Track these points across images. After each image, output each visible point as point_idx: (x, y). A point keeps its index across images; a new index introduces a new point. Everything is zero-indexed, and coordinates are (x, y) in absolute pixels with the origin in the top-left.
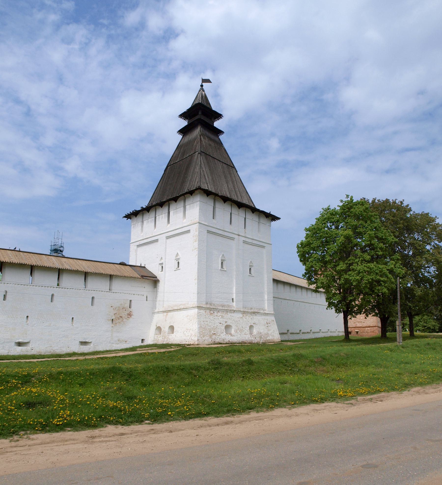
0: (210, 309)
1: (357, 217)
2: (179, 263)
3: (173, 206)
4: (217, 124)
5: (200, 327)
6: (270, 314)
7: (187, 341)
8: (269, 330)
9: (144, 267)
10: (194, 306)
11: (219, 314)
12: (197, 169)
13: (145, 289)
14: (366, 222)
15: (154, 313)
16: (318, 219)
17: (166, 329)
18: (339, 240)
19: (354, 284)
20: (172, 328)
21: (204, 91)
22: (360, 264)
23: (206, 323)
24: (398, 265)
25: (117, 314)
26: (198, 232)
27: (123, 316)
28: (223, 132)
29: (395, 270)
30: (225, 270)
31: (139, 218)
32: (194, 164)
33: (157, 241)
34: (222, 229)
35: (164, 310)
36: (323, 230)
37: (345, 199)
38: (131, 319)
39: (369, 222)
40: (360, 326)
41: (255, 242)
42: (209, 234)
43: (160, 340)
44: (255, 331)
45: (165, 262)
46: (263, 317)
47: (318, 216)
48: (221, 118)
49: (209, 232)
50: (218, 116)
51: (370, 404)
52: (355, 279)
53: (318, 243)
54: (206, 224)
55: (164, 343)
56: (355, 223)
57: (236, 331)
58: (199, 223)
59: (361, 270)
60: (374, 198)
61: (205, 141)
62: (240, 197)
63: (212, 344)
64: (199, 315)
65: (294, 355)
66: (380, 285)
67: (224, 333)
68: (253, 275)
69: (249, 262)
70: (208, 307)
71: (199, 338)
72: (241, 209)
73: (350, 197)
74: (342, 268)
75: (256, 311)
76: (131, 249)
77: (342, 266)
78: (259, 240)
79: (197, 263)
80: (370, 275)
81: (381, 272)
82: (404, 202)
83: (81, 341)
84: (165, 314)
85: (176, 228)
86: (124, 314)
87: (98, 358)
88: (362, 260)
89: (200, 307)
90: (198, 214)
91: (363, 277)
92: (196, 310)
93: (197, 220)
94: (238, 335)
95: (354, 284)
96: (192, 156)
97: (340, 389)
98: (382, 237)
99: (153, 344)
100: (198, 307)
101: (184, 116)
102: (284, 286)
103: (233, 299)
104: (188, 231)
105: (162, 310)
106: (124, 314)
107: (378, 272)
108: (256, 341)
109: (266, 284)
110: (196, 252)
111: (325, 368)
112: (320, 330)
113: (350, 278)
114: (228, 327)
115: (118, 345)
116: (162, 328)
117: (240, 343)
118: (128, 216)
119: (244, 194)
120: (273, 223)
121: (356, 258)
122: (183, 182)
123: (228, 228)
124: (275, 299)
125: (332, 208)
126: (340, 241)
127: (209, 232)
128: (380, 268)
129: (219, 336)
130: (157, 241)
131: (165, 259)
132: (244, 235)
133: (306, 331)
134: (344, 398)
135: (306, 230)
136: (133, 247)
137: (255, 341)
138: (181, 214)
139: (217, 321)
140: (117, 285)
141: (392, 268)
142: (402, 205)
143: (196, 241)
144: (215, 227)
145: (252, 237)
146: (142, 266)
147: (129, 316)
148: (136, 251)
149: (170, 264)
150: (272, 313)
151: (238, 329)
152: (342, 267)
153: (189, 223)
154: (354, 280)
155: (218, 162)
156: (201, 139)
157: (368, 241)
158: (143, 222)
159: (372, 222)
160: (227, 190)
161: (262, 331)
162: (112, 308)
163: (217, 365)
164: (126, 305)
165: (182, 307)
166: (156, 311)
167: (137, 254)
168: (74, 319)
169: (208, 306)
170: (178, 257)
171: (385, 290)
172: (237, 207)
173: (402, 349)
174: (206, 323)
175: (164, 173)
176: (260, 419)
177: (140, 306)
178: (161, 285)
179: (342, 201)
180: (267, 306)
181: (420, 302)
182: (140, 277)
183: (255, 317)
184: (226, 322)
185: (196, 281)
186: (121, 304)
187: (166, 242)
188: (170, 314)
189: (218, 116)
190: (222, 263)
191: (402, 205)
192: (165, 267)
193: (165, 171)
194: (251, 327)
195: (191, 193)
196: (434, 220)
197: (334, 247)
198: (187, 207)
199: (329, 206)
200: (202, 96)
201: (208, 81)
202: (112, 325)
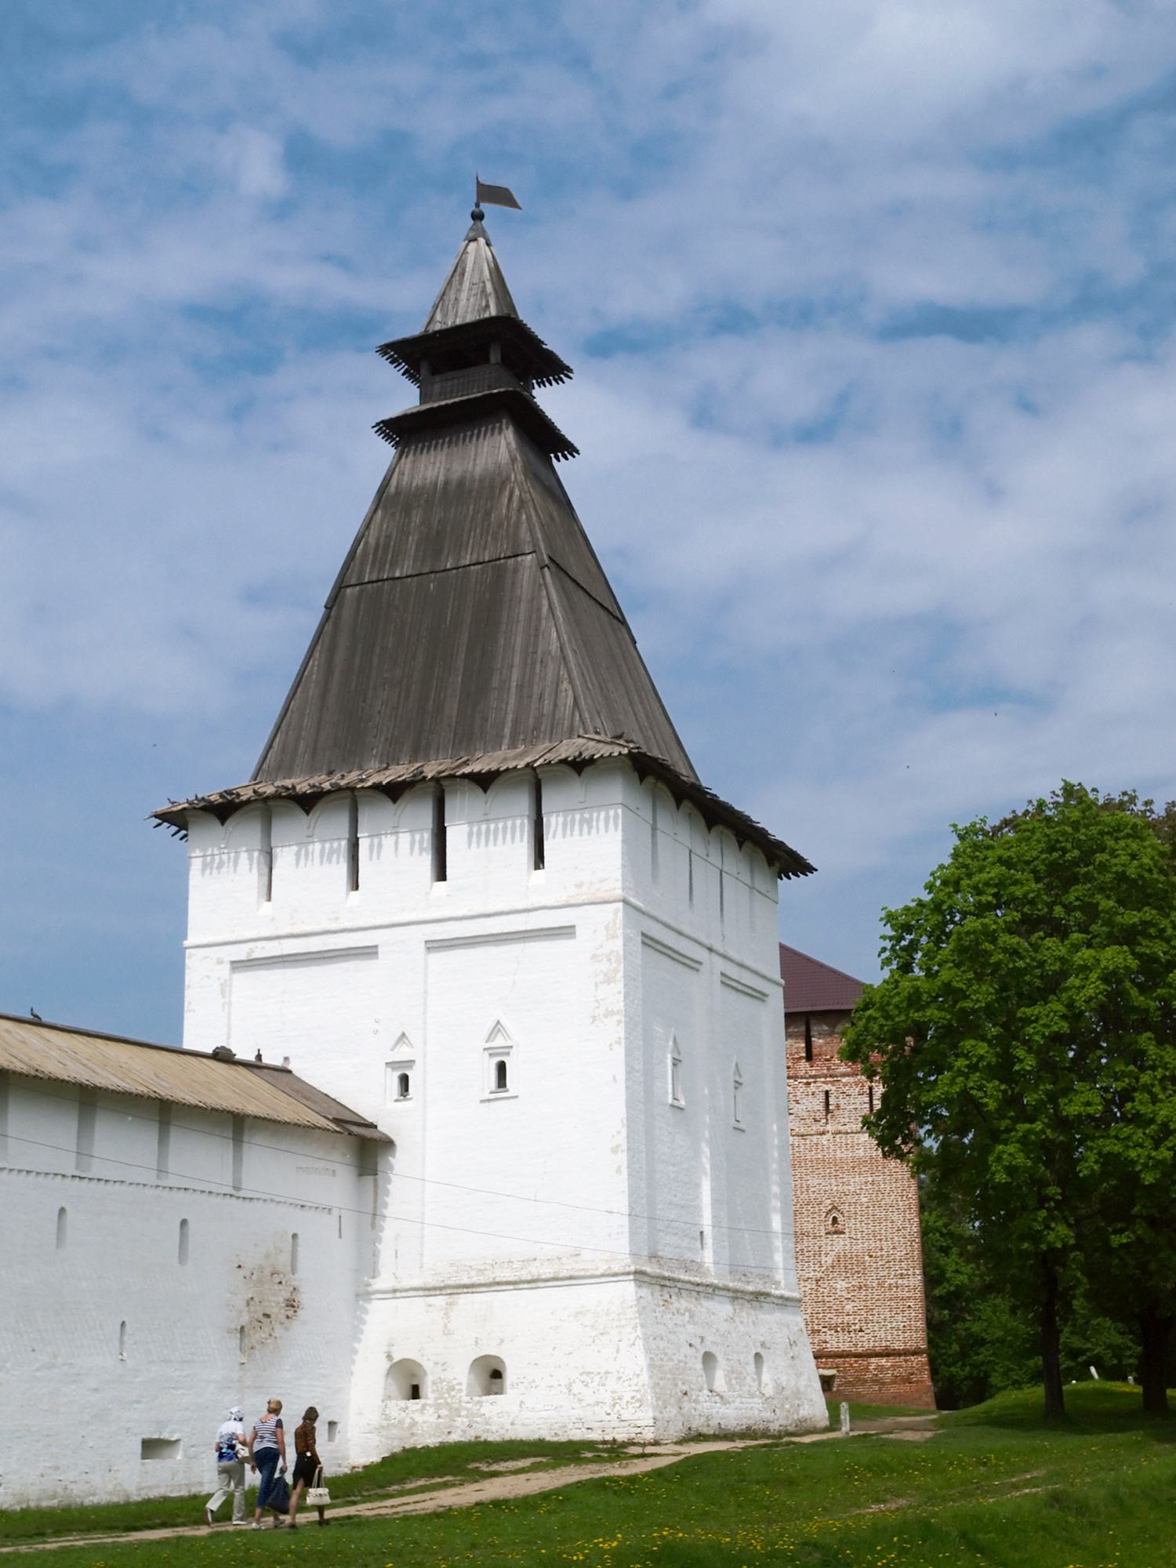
2: (502, 1068)
5: (652, 1366)
10: (616, 1268)
13: (329, 1179)
19: (1148, 1178)
20: (493, 1375)
40: (845, 1347)
42: (648, 949)
43: (428, 1425)
48: (559, 380)
52: (1150, 1157)
53: (983, 994)
54: (640, 904)
55: (455, 1437)
56: (1131, 918)
58: (625, 902)
70: (662, 1280)
71: (657, 1414)
83: (147, 1436)
84: (440, 1301)
85: (490, 909)
88: (1164, 1077)
92: (628, 1289)
95: (1148, 1178)
96: (498, 571)
100: (636, 1273)
104: (566, 932)
113: (1133, 1154)
118: (178, 819)
136: (202, 975)
143: (609, 980)
146: (266, 1060)
147: (291, 1313)
148: (225, 989)
149: (452, 1074)
152: (1088, 1104)
153: (563, 899)
154: (1145, 1165)
162: (242, 1272)
165: (547, 1271)
166: (378, 1284)
168: (128, 1329)
170: (499, 1041)
172: (703, 821)
175: (326, 618)
177: (322, 1269)
178: (400, 1164)
185: (622, 1158)
186: (267, 1256)
188: (464, 1300)
189: (553, 369)
193: (329, 607)
197: (1047, 1017)
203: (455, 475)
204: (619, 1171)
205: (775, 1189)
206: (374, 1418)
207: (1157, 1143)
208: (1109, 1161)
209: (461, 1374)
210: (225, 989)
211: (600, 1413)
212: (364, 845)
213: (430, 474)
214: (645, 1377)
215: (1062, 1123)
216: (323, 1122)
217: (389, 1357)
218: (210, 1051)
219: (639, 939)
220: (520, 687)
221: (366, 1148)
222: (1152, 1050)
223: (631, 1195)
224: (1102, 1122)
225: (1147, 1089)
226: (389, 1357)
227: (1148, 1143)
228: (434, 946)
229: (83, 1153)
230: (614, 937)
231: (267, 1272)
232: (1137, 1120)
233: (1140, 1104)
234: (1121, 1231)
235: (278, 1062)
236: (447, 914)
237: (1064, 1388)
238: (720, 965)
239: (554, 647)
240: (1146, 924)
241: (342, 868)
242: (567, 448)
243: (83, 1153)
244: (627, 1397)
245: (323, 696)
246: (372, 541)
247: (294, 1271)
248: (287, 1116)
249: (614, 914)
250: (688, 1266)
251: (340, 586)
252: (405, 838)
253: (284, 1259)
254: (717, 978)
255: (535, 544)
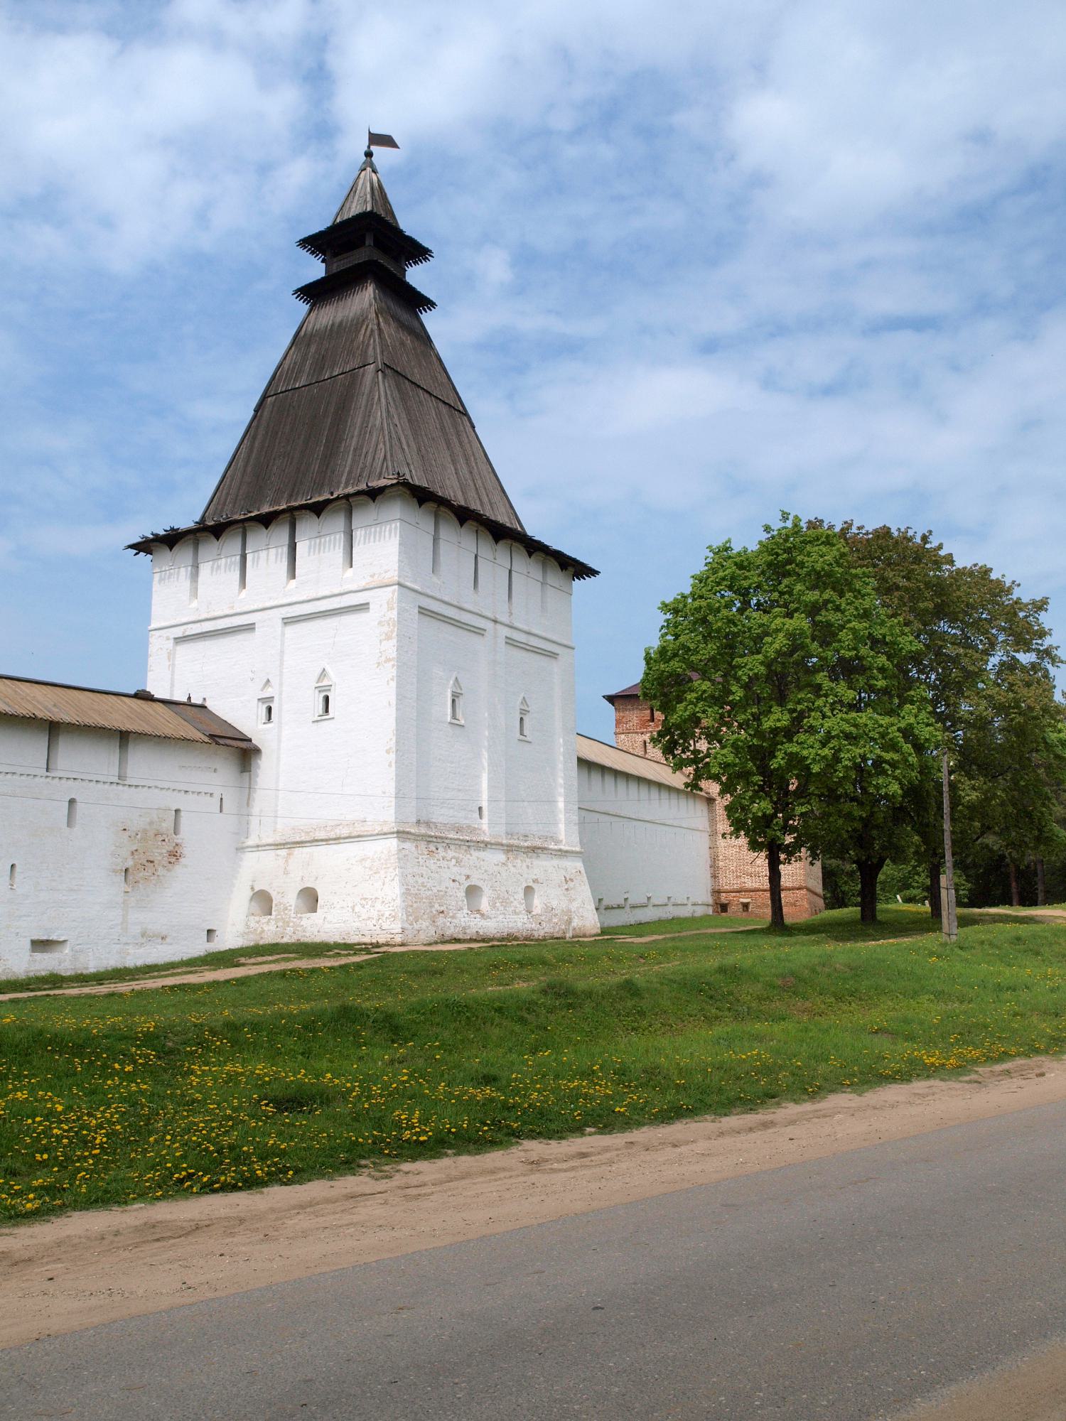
0: (428, 839)
1: (819, 580)
2: (327, 699)
3: (307, 530)
4: (416, 276)
5: (407, 893)
6: (572, 852)
7: (366, 933)
8: (571, 900)
9: (203, 707)
11: (451, 854)
12: (379, 416)
13: (215, 776)
14: (841, 595)
15: (241, 849)
16: (701, 579)
17: (287, 898)
18: (771, 644)
19: (816, 769)
20: (310, 899)
21: (374, 171)
22: (829, 714)
23: (420, 880)
24: (923, 715)
25: (141, 851)
26: (395, 612)
27: (157, 858)
28: (433, 304)
29: (916, 732)
30: (462, 722)
31: (183, 554)
32: (363, 401)
33: (250, 628)
34: (455, 603)
35: (278, 839)
36: (724, 612)
37: (777, 525)
38: (178, 869)
39: (849, 595)
41: (534, 642)
43: (270, 931)
44: (538, 904)
45: (281, 694)
46: (556, 862)
47: (699, 567)
48: (426, 259)
49: (423, 611)
50: (418, 252)
51: (1007, 1084)
53: (711, 649)
54: (416, 587)
56: (813, 596)
57: (494, 906)
58: (399, 584)
59: (833, 729)
60: (848, 520)
61: (390, 330)
62: (488, 507)
63: (436, 943)
64: (402, 857)
65: (722, 970)
66: (884, 772)
67: (466, 911)
68: (528, 739)
69: (520, 699)
70: (423, 835)
71: (406, 926)
72: (501, 543)
73: (791, 517)
74: (778, 724)
75: (538, 843)
76: (152, 649)
77: (778, 718)
78: (543, 634)
79: (394, 702)
80: (856, 745)
81: (883, 736)
82: (931, 538)
83: (35, 938)
84: (283, 852)
85: (320, 595)
86: (159, 853)
87: (172, 988)
88: (835, 702)
89: (404, 832)
90: (396, 558)
91: (840, 750)
92: (393, 843)
93: (393, 575)
94: (500, 917)
95: (816, 769)
96: (353, 376)
97: (897, 1052)
98: (884, 637)
99: (242, 949)
100: (398, 832)
101: (314, 243)
102: (589, 772)
103: (480, 808)
104: (363, 607)
105: (270, 841)
106: (159, 853)
107: (877, 736)
108: (542, 933)
109: (560, 766)
110: (391, 671)
111: (808, 1004)
112: (649, 898)
113: (805, 753)
114: (472, 892)
115: (142, 950)
116: (274, 894)
117: (503, 939)
118: (144, 546)
119: (497, 497)
120: (577, 583)
121: (819, 696)
122: (331, 453)
123: (469, 599)
124: (583, 813)
125: (737, 548)
126: (776, 646)
127: (423, 611)
128: (881, 726)
129: (453, 917)
130: (250, 628)
131: (281, 684)
132: (507, 622)
133: (614, 903)
134: (960, 1070)
135: (665, 607)
136: (159, 645)
137: (540, 933)
138: (338, 553)
139: (447, 872)
140: (142, 763)
141: (911, 724)
142: (928, 546)
143: (388, 638)
144: (438, 595)
145: (526, 628)
146: (193, 701)
147: (173, 860)
148: (171, 656)
149: (297, 702)
150: (578, 849)
151: (498, 898)
152: (779, 720)
153: (362, 584)
154: (814, 759)
155: (427, 396)
156: (379, 324)
157: (849, 650)
158: (196, 567)
159: (859, 594)
160: (456, 484)
161: (554, 903)
162: (127, 833)
163: (563, 995)
164: (164, 825)
165: (345, 832)
166: (251, 842)
167: (173, 665)
168: (18, 869)
169: (423, 830)
170: (325, 683)
171: (895, 788)
173: (960, 952)
174: (420, 880)
176: (825, 1116)
177: (202, 829)
178: (265, 767)
179: (767, 529)
180: (565, 832)
181: (971, 819)
182: (207, 740)
183: (536, 862)
184: (468, 877)
185: (393, 756)
186: (151, 823)
187: (283, 634)
188: (298, 852)
189: (418, 252)
190: (453, 701)
191: (928, 546)
192: (280, 710)
193: (256, 411)
194: (529, 890)
195: (374, 494)
196: (1009, 591)
197: (752, 665)
198: (358, 534)
199: (729, 541)
200: (372, 188)
201: (387, 141)
202: (124, 887)
203: (338, 320)
204: (390, 765)
205: (561, 781)
206: (241, 928)
207: (824, 745)
208: (791, 756)
209: (291, 899)
210: (171, 656)
211: (370, 924)
212: (249, 557)
213: (324, 322)
214: (399, 901)
215: (759, 734)
216: (198, 735)
217: (252, 888)
218: (132, 692)
219: (416, 610)
220: (355, 450)
221: (244, 753)
222: (827, 684)
223: (398, 781)
224: (789, 734)
225: (819, 709)
226: (252, 888)
227: (817, 745)
228: (288, 621)
229: (122, 762)
230: (392, 609)
231: (151, 834)
232: (812, 730)
233: (813, 720)
234: (802, 805)
235: (199, 702)
236: (294, 599)
237: (880, 906)
238: (505, 632)
239: (378, 422)
240: (826, 602)
241: (236, 574)
242: (427, 303)
243: (122, 762)
244: (387, 914)
245: (246, 466)
246: (286, 367)
247: (176, 832)
248: (168, 731)
249: (391, 593)
250: (473, 830)
251: (264, 397)
252: (273, 551)
253: (168, 825)
254: (502, 641)
255: (376, 358)
